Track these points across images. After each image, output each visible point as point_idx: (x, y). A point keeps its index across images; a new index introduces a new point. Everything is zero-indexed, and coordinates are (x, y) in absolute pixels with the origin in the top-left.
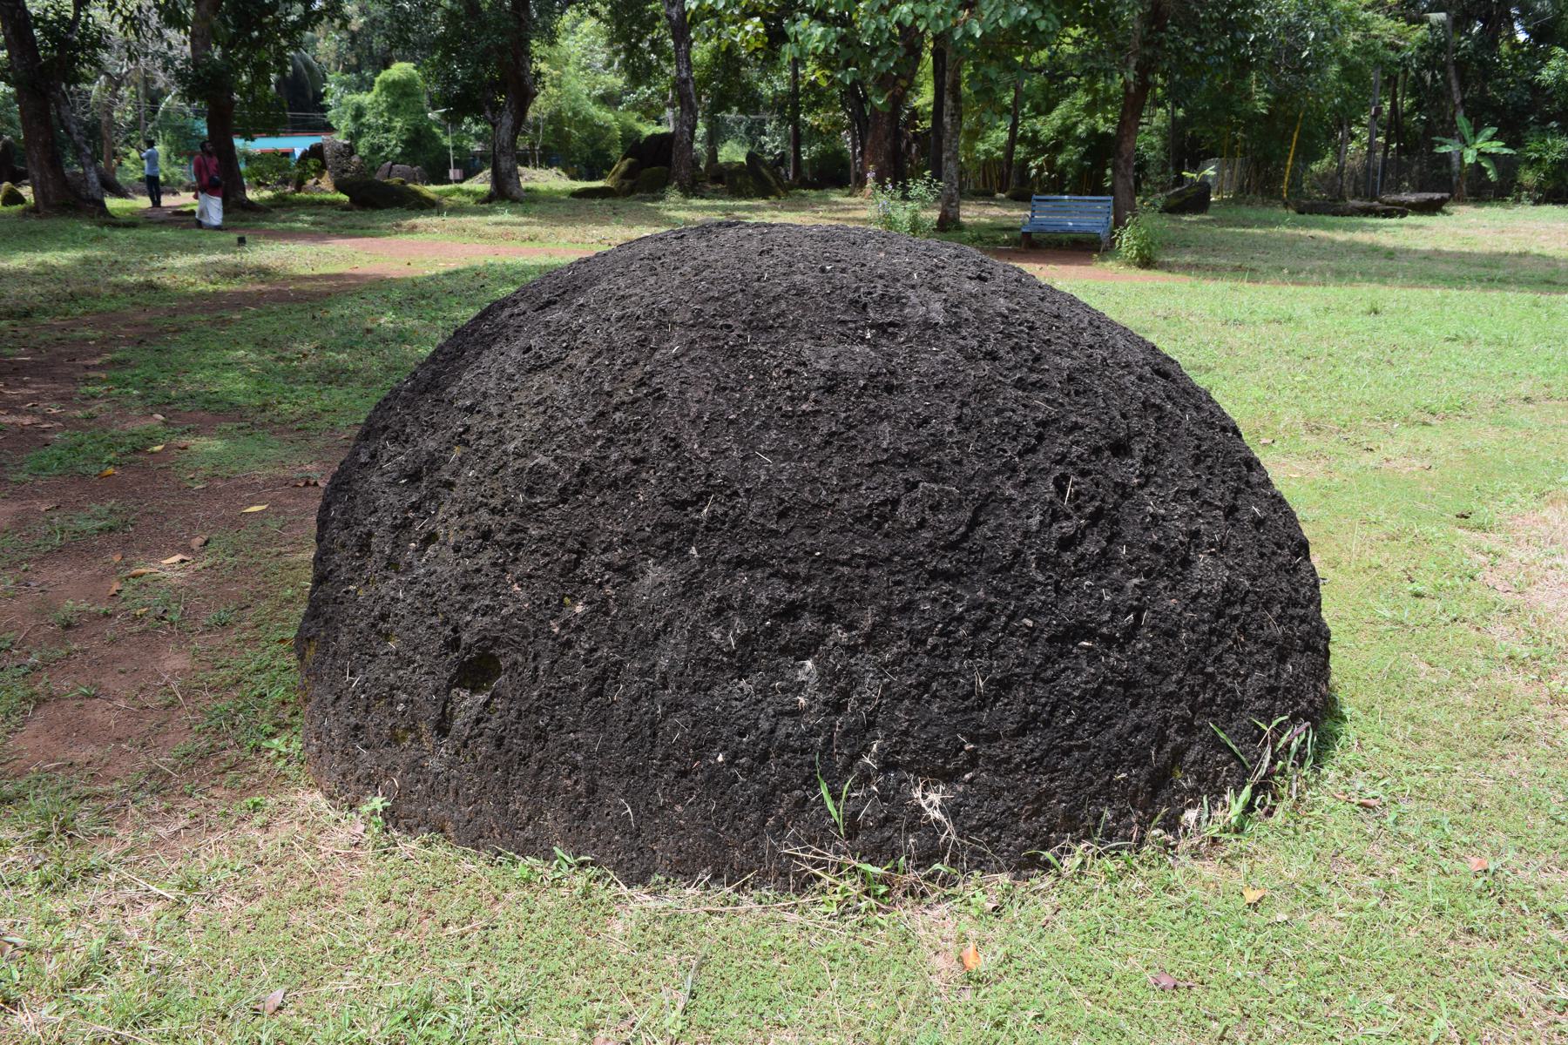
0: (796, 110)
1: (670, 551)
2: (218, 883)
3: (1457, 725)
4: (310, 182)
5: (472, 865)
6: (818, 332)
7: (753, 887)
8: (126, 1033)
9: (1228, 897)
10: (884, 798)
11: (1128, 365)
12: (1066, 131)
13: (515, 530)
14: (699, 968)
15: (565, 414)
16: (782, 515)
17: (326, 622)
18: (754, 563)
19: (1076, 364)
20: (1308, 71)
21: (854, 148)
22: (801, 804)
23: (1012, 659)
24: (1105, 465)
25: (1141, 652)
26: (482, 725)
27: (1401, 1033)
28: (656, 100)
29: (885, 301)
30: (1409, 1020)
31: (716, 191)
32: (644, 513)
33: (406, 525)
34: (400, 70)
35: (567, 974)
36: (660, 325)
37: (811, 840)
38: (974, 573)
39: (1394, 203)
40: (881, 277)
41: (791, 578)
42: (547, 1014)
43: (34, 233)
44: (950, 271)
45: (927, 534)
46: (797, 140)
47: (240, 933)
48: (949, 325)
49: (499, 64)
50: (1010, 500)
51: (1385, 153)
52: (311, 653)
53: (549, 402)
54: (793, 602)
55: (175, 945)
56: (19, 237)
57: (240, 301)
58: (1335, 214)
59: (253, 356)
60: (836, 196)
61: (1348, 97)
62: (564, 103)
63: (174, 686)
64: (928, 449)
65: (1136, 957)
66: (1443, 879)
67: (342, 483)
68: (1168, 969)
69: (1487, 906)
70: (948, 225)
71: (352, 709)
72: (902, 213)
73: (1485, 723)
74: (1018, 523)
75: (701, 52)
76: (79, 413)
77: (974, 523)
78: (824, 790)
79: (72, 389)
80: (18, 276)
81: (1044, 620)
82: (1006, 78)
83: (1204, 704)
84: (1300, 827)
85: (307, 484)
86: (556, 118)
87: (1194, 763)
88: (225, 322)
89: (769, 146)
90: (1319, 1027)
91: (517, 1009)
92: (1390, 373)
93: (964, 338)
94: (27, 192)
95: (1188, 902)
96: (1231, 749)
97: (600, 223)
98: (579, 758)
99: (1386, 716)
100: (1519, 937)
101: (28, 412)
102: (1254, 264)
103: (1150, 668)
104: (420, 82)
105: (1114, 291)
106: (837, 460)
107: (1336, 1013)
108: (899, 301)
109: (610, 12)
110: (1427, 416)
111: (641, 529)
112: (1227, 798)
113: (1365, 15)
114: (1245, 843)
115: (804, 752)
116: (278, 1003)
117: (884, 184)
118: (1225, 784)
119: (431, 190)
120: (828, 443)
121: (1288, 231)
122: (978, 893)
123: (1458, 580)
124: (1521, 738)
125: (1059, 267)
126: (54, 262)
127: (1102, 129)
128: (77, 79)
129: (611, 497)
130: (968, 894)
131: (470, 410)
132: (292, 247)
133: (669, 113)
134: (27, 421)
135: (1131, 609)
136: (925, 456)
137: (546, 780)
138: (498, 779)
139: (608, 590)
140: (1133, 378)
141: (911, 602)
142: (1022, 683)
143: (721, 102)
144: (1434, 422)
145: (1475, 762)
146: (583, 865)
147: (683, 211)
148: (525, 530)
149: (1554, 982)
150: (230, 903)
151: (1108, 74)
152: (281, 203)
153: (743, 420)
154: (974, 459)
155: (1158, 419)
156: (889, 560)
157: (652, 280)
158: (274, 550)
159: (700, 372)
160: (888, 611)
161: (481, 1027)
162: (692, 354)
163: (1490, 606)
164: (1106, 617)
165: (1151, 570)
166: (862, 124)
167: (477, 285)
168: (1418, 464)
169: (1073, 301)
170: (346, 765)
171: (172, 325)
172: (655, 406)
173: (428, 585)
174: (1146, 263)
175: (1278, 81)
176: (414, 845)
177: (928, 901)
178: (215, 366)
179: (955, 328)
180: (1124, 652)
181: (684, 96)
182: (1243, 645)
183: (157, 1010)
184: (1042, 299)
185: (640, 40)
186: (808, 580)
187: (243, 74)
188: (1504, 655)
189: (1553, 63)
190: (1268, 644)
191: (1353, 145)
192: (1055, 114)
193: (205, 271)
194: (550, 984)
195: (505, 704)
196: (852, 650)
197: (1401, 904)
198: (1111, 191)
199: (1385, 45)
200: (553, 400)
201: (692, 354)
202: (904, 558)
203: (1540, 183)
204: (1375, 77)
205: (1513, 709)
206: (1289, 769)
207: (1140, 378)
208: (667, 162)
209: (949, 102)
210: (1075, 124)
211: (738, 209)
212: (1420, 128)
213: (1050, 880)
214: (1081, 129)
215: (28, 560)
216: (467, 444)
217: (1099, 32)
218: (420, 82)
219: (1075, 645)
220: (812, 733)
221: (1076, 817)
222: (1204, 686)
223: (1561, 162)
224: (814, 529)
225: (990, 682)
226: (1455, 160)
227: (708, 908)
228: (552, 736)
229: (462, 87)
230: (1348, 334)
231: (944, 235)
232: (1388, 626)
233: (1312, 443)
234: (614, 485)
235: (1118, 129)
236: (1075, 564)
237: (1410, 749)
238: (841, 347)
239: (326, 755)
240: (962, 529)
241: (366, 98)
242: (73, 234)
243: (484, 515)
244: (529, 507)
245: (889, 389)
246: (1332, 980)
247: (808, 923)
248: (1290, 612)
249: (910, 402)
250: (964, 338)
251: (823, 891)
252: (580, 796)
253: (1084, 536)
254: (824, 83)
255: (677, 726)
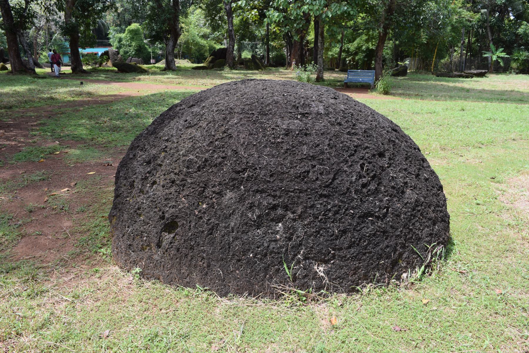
0: (268, 40)
1: (234, 188)
2: (85, 296)
3: (491, 247)
4: (104, 64)
5: (169, 290)
6: (282, 116)
7: (262, 298)
8: (58, 344)
9: (417, 302)
10: (305, 269)
11: (383, 127)
12: (359, 48)
13: (183, 180)
14: (245, 324)
15: (199, 142)
16: (271, 176)
17: (119, 210)
18: (262, 192)
19: (367, 127)
20: (440, 29)
21: (287, 53)
22: (278, 270)
23: (347, 224)
24: (377, 160)
25: (389, 222)
26: (172, 244)
27: (474, 345)
28: (221, 37)
29: (304, 105)
30: (476, 341)
31: (241, 68)
32: (226, 175)
33: (146, 178)
34: (134, 26)
35: (202, 325)
36: (230, 113)
37: (281, 282)
38: (334, 195)
39: (469, 73)
40: (303, 98)
41: (274, 196)
42: (196, 338)
43: (12, 80)
44: (325, 96)
45: (319, 182)
46: (268, 51)
47: (93, 312)
48: (325, 114)
49: (168, 25)
50: (346, 171)
51: (466, 57)
52: (114, 221)
53: (194, 138)
54: (275, 204)
55: (72, 316)
56: (6, 81)
57: (82, 104)
58: (449, 77)
59: (88, 122)
60: (281, 70)
61: (453, 38)
62: (190, 38)
63: (67, 231)
64: (319, 154)
65: (388, 321)
66: (487, 296)
67: (124, 164)
68: (398, 324)
69: (502, 305)
70: (319, 79)
71: (128, 239)
72: (304, 76)
73: (500, 246)
74: (348, 179)
75: (236, 21)
76: (30, 141)
77: (334, 179)
78: (285, 266)
79: (28, 133)
80: (7, 94)
81: (357, 211)
82: (339, 30)
83: (409, 239)
84: (440, 279)
85: (108, 165)
86: (187, 43)
87: (406, 258)
88: (78, 111)
89: (259, 52)
90: (447, 343)
91: (186, 337)
92: (468, 130)
93: (330, 118)
94: (9, 66)
95: (404, 303)
96: (418, 254)
97: (202, 78)
98: (205, 255)
99: (468, 243)
100: (512, 315)
101: (13, 140)
102: (422, 94)
103: (392, 227)
104: (141, 30)
105: (375, 102)
106: (289, 158)
107: (453, 339)
108: (309, 105)
109: (206, 7)
110: (481, 145)
111: (225, 180)
112: (416, 270)
113: (459, 10)
114: (422, 284)
115: (279, 253)
116: (107, 335)
117: (298, 66)
118: (416, 265)
119: (145, 66)
120: (286, 152)
121: (433, 83)
122: (336, 300)
123: (491, 199)
124: (513, 251)
125: (357, 94)
126: (19, 90)
127: (371, 48)
128: (26, 28)
129: (215, 170)
130: (332, 300)
131: (167, 140)
132: (99, 85)
133: (225, 41)
134: (13, 143)
135: (385, 207)
136: (318, 157)
137: (194, 262)
138: (178, 262)
139: (214, 200)
140: (385, 132)
141: (314, 205)
142: (350, 231)
143: (243, 38)
144: (483, 147)
145: (497, 259)
146: (206, 290)
147: (230, 76)
148: (186, 180)
149: (524, 329)
150: (90, 303)
151: (373, 30)
152: (94, 71)
153: (258, 145)
154: (334, 158)
155: (393, 145)
156: (306, 191)
157: (227, 98)
158: (99, 187)
159: (244, 129)
160: (306, 207)
161: (174, 342)
162: (241, 123)
163: (502, 208)
164: (377, 210)
165: (392, 195)
166: (290, 44)
167: (162, 99)
168: (478, 161)
169: (365, 106)
170: (126, 258)
171: (60, 111)
172: (229, 140)
173: (154, 198)
174: (386, 93)
175: (430, 32)
176: (149, 284)
177: (319, 302)
178: (75, 125)
179: (327, 115)
180: (386, 222)
181: (231, 37)
182: (422, 220)
183: (68, 337)
184: (355, 105)
185: (215, 16)
186: (280, 197)
187: (82, 26)
188: (507, 224)
189: (523, 27)
190: (430, 219)
191: (455, 54)
192: (355, 42)
193: (70, 93)
194: (196, 329)
195: (180, 237)
196: (294, 220)
197: (474, 304)
198: (374, 69)
199: (466, 20)
200: (195, 137)
201: (241, 123)
202: (311, 190)
203: (518, 67)
204: (463, 31)
205: (510, 241)
206: (437, 260)
207: (388, 132)
208: (225, 58)
209: (320, 38)
210: (362, 46)
211: (249, 74)
212: (478, 48)
213: (359, 296)
214: (364, 47)
215: (16, 190)
216: (166, 152)
217: (371, 15)
218: (141, 30)
219: (367, 219)
220: (281, 247)
221: (367, 275)
222: (409, 233)
223: (525, 60)
224: (282, 180)
225: (339, 231)
226: (490, 59)
227: (247, 304)
228: (195, 248)
229: (156, 32)
230: (454, 117)
231: (318, 83)
232: (468, 214)
233: (442, 153)
234: (216, 165)
235: (377, 48)
236: (367, 193)
237: (476, 254)
238: (290, 121)
239: (120, 254)
240: (330, 181)
241: (123, 35)
242: (25, 80)
243: (172, 175)
244: (187, 173)
245: (306, 135)
246: (451, 328)
247: (280, 310)
248: (437, 209)
249: (313, 139)
250: (330, 118)
251: (285, 299)
252: (205, 267)
253: (370, 183)
254: (278, 32)
255: (237, 245)
